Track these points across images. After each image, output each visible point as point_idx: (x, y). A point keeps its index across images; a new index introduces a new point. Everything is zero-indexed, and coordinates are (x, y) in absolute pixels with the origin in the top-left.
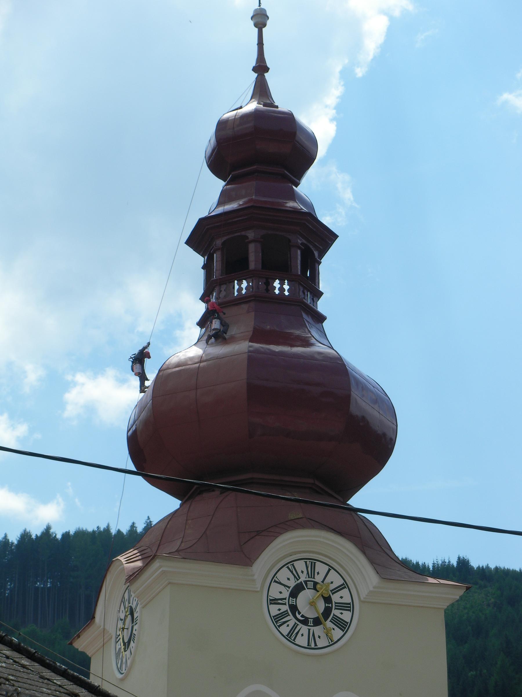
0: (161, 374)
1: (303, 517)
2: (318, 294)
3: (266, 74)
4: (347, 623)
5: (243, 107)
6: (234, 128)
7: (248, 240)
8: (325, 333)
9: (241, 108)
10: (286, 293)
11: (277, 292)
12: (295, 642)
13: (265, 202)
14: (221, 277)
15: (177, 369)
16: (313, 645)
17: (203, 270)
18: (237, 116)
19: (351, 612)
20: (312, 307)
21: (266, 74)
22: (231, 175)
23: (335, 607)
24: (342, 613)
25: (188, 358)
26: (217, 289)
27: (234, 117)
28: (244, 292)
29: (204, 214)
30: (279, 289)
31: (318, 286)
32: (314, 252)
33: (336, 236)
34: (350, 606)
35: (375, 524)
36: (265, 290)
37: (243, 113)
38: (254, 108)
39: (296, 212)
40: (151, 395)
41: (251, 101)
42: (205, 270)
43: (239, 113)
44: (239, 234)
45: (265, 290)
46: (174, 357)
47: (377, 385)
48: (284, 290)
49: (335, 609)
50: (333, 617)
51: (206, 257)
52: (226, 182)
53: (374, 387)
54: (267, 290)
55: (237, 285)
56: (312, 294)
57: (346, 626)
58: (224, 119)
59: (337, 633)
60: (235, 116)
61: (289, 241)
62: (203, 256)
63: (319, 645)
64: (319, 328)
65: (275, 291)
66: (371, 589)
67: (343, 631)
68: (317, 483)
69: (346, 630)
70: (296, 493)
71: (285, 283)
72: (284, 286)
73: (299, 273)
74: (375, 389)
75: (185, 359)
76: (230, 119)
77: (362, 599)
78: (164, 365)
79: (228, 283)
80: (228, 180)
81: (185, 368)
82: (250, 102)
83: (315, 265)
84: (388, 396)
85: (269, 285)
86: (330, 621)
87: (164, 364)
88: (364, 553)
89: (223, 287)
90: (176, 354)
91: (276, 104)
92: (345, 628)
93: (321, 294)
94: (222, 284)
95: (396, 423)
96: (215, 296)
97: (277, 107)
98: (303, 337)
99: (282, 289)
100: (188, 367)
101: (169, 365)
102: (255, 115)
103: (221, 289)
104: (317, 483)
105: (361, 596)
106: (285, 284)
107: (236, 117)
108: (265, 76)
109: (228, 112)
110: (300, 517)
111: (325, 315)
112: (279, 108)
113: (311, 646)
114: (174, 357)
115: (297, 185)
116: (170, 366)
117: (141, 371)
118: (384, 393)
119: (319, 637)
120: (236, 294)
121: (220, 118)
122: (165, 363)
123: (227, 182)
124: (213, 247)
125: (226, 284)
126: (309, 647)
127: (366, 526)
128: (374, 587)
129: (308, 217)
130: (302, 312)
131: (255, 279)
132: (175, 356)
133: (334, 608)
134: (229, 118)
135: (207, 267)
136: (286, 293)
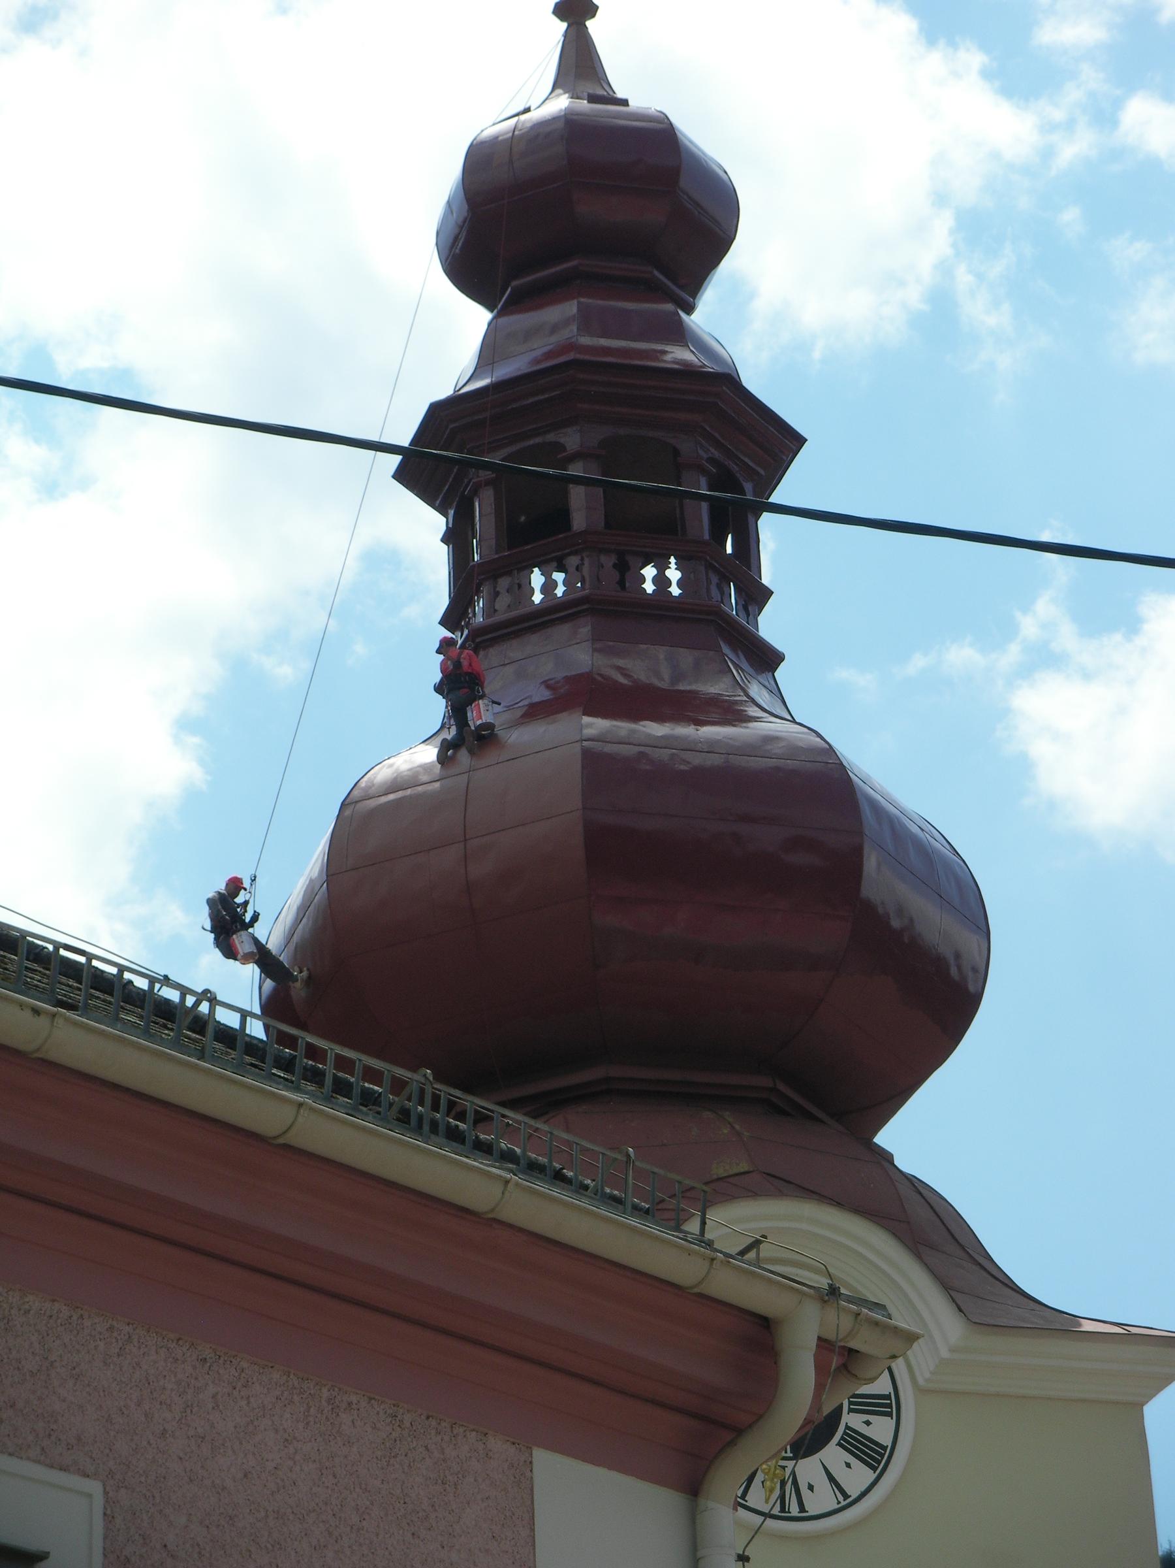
0: (348, 813)
1: (751, 1169)
2: (757, 596)
3: (589, 23)
4: (884, 1448)
5: (532, 109)
6: (511, 162)
7: (564, 454)
8: (783, 698)
9: (527, 110)
10: (675, 591)
11: (649, 587)
12: (746, 1501)
13: (607, 351)
14: (496, 556)
15: (392, 797)
16: (794, 1510)
17: (447, 547)
18: (521, 130)
19: (892, 1419)
20: (743, 627)
21: (589, 23)
22: (509, 290)
23: (849, 1406)
24: (868, 1423)
25: (420, 766)
26: (485, 589)
27: (511, 134)
28: (560, 591)
29: (444, 392)
30: (655, 580)
31: (758, 575)
32: (744, 484)
33: (800, 441)
34: (889, 1402)
35: (941, 1194)
36: (617, 583)
37: (535, 122)
38: (564, 108)
39: (688, 373)
40: (325, 870)
41: (553, 95)
42: (451, 546)
43: (524, 122)
44: (538, 440)
45: (617, 583)
46: (381, 769)
47: (933, 828)
48: (669, 583)
49: (850, 1411)
50: (845, 1433)
51: (451, 512)
52: (495, 311)
53: (922, 830)
54: (622, 583)
55: (541, 574)
56: (743, 594)
57: (882, 1456)
58: (484, 140)
59: (857, 1477)
60: (514, 131)
61: (676, 452)
62: (442, 510)
63: (812, 1509)
64: (766, 684)
65: (643, 586)
66: (945, 1353)
67: (874, 1469)
68: (781, 1087)
69: (896, 1403)
70: (728, 1113)
71: (670, 563)
72: (668, 573)
73: (707, 537)
74: (927, 836)
75: (409, 770)
76: (500, 138)
77: (921, 1381)
78: (354, 789)
79: (516, 571)
80: (499, 306)
81: (413, 793)
82: (550, 97)
83: (747, 517)
84: (958, 853)
85: (629, 569)
86: (839, 1444)
87: (356, 787)
88: (918, 1256)
89: (504, 583)
90: (387, 761)
91: (620, 94)
92: (879, 1462)
93: (766, 594)
94: (501, 575)
95: (985, 927)
96: (483, 608)
97: (625, 103)
98: (726, 701)
99: (661, 581)
100: (420, 789)
101: (368, 787)
102: (569, 124)
103: (498, 589)
104: (781, 1087)
105: (917, 1373)
106: (670, 568)
107: (516, 133)
108: (587, 28)
109: (494, 124)
110: (742, 1170)
111: (780, 650)
112: (630, 107)
113: (790, 1513)
114: (381, 769)
115: (690, 309)
116: (372, 792)
117: (254, 947)
118: (949, 848)
119: (811, 1488)
120: (537, 598)
121: (475, 139)
122: (358, 785)
123: (498, 312)
124: (471, 480)
125: (509, 573)
126: (783, 1514)
127: (921, 1194)
128: (952, 1350)
129: (724, 388)
130: (722, 644)
131: (588, 557)
132: (384, 766)
133: (847, 1410)
134: (497, 137)
135: (455, 538)
136: (675, 591)
